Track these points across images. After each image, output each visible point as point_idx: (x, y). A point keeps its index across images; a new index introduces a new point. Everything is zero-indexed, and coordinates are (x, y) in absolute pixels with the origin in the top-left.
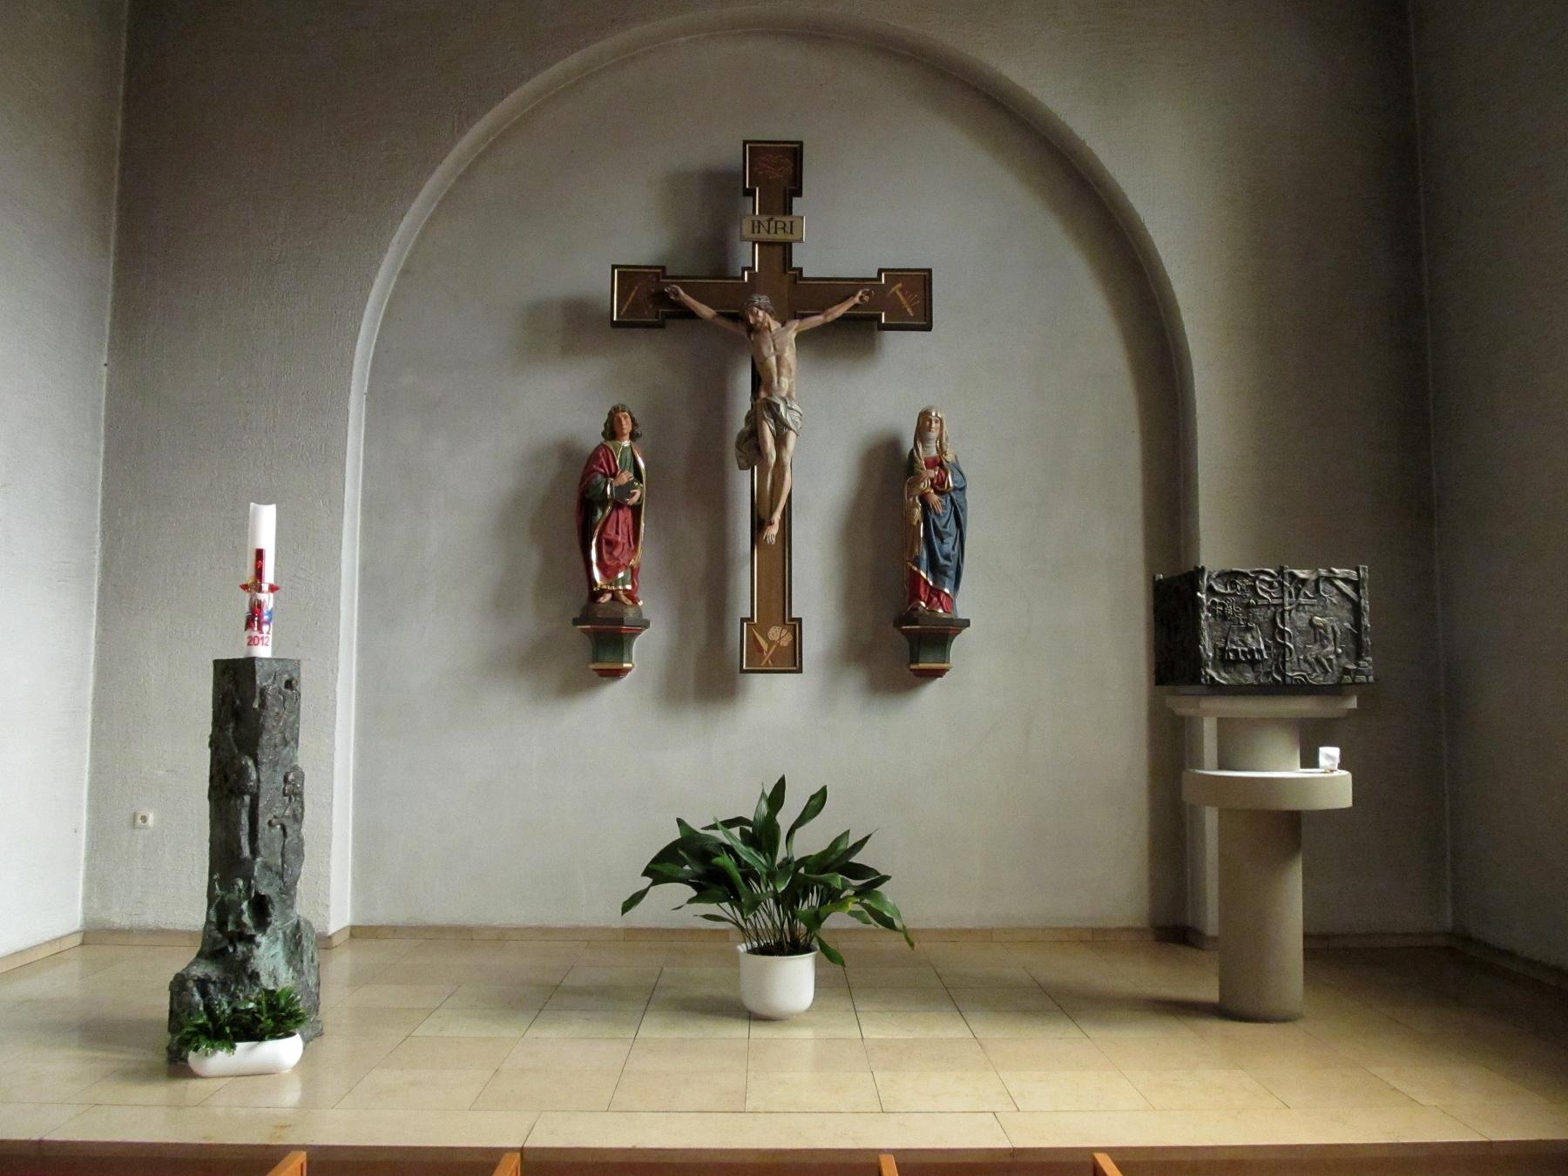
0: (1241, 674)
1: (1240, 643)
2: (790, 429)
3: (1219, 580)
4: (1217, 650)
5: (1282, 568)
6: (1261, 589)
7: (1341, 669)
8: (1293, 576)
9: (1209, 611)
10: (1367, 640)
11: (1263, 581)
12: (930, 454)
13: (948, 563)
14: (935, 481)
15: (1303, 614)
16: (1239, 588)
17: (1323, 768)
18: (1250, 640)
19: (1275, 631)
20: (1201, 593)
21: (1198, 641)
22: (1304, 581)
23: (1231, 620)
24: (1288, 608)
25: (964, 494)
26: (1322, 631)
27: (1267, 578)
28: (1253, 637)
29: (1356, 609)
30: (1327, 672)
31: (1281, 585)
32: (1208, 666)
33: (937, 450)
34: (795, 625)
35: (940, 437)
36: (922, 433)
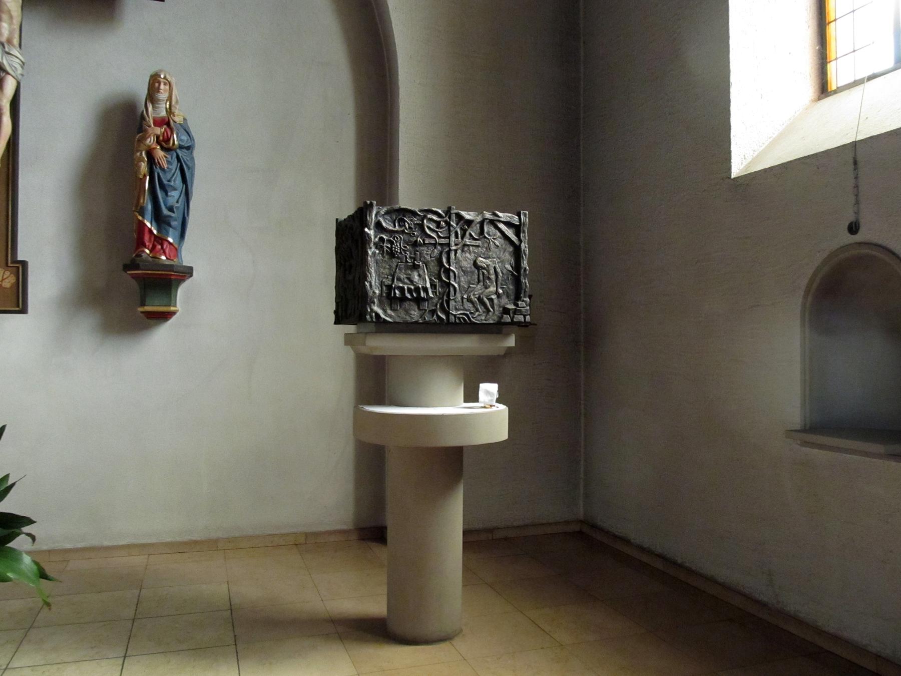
0: (407, 312)
1: (406, 280)
2: (8, 73)
3: (387, 217)
4: (384, 288)
5: (450, 208)
6: (429, 228)
7: (501, 309)
8: (460, 217)
9: (376, 248)
10: (525, 281)
11: (431, 220)
12: (159, 114)
13: (173, 215)
14: (161, 138)
15: (468, 255)
16: (407, 226)
17: (482, 403)
18: (416, 278)
19: (442, 271)
20: (369, 229)
21: (365, 278)
22: (469, 223)
23: (398, 258)
24: (454, 248)
25: (192, 153)
26: (485, 271)
27: (435, 218)
28: (419, 276)
29: (517, 252)
30: (488, 311)
31: (448, 224)
32: (374, 303)
33: (167, 111)
34: (18, 268)
35: (170, 98)
36: (152, 96)
